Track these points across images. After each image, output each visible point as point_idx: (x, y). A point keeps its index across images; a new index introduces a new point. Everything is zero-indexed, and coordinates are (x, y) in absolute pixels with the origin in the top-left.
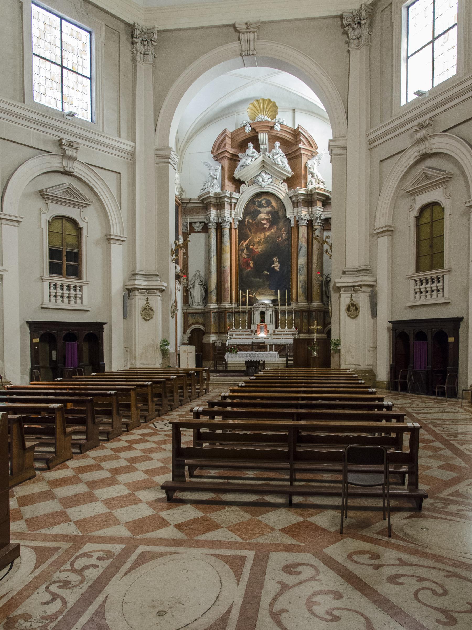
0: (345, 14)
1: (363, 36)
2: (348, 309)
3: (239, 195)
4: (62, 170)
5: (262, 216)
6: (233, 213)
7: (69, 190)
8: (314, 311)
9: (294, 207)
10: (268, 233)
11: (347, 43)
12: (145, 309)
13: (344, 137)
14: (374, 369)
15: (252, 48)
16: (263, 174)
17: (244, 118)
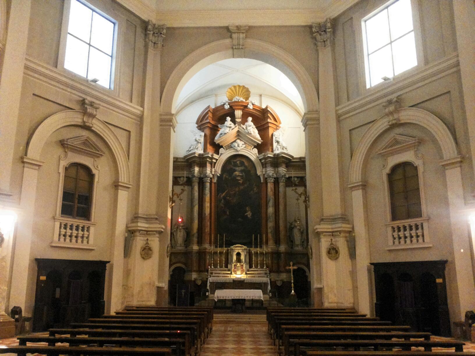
0: (314, 25)
1: (328, 40)
2: (329, 253)
3: (218, 156)
4: (82, 124)
5: (237, 173)
6: (213, 170)
7: (86, 142)
8: (283, 253)
9: (263, 168)
10: (242, 187)
11: (316, 44)
12: (144, 249)
13: (316, 111)
14: (356, 307)
15: (241, 43)
16: (238, 141)
17: (222, 99)
